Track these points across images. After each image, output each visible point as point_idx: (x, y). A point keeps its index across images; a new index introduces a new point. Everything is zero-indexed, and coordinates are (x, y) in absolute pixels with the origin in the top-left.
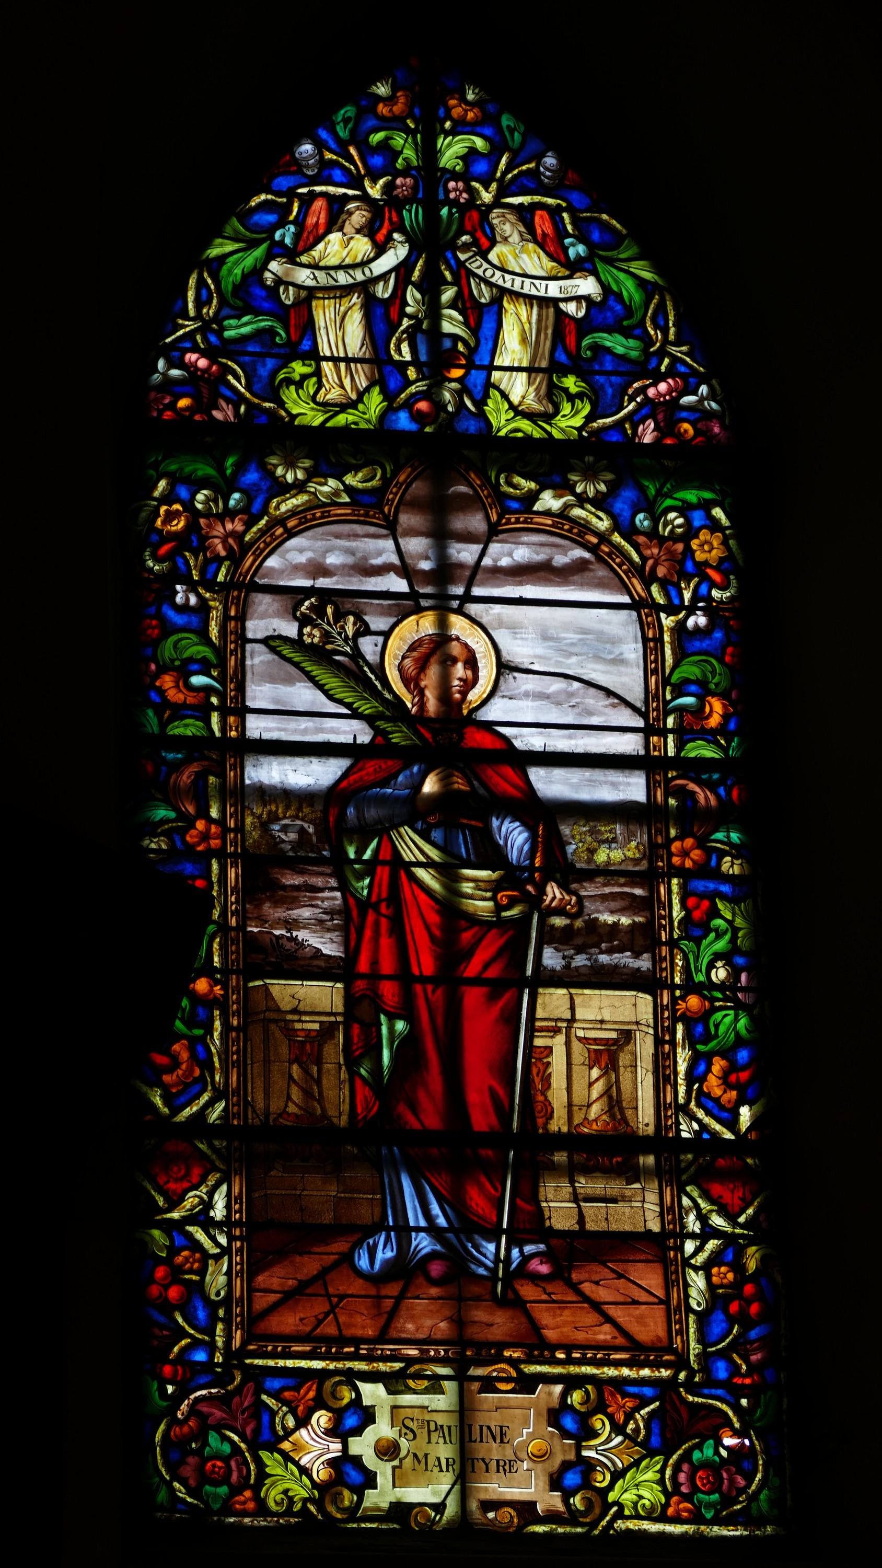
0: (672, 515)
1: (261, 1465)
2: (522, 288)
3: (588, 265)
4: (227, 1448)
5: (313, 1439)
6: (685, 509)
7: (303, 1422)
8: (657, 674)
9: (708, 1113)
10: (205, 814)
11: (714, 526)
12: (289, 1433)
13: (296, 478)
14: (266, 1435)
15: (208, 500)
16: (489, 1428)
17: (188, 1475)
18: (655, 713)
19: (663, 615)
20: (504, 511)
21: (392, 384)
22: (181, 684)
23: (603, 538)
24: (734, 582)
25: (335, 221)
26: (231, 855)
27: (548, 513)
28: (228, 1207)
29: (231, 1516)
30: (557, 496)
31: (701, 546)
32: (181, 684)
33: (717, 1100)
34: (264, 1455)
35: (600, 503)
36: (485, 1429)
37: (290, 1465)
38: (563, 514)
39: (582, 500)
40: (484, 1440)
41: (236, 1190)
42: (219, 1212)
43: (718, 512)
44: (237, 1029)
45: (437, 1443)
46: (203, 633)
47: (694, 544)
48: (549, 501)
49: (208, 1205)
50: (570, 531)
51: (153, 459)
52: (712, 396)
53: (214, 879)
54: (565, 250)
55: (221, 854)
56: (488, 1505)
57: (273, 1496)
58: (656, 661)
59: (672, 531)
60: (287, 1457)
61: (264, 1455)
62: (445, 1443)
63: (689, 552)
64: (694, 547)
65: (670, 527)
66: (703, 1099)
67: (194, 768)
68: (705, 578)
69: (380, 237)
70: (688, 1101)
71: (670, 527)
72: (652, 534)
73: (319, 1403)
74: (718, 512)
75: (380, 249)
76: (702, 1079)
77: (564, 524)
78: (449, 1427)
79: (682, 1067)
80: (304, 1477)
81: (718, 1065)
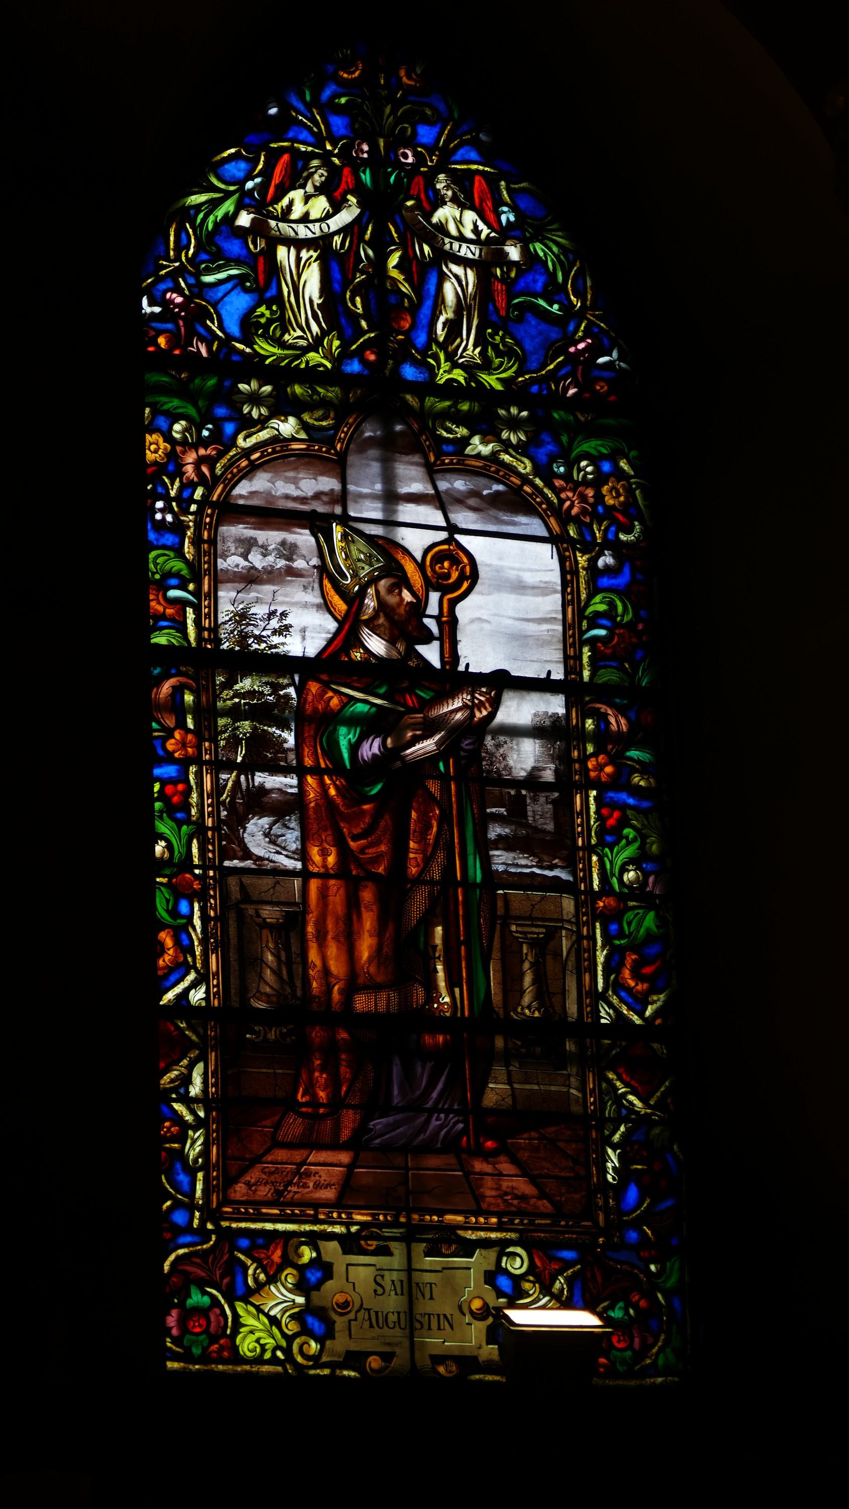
0: (584, 463)
1: (236, 1316)
2: (459, 251)
3: (517, 233)
4: (206, 1300)
5: (283, 1295)
6: (594, 460)
7: (273, 1279)
8: (573, 605)
9: (622, 1000)
10: (182, 724)
11: (619, 474)
12: (260, 1286)
13: (261, 414)
14: (240, 1291)
15: (185, 430)
16: (445, 1316)
17: (172, 1324)
18: (571, 640)
19: (578, 554)
20: (439, 454)
21: (349, 332)
22: (160, 596)
23: (524, 479)
24: (638, 527)
25: (295, 180)
26: (207, 763)
27: (478, 456)
28: (205, 1082)
29: (187, 960)
30: (484, 442)
31: (610, 491)
32: (160, 596)
33: (629, 990)
34: (240, 1307)
35: (522, 449)
36: (442, 1317)
37: (261, 1316)
38: (493, 457)
39: (507, 445)
40: (442, 1327)
41: (211, 1068)
42: (195, 1090)
43: (623, 464)
44: (215, 919)
45: (389, 1295)
46: (180, 554)
47: (605, 489)
48: (479, 446)
49: (187, 1080)
50: (497, 472)
51: (303, 1076)
52: (620, 359)
53: (192, 782)
54: (498, 215)
55: (198, 761)
56: (438, 1359)
57: (247, 1345)
58: (572, 593)
59: (585, 476)
60: (259, 1309)
61: (240, 1307)
62: (396, 1294)
63: (599, 497)
64: (604, 493)
65: (582, 473)
66: (618, 986)
67: (172, 681)
68: (614, 521)
69: (337, 194)
70: (606, 989)
71: (582, 473)
72: (567, 477)
73: (287, 1262)
74: (623, 464)
75: (337, 206)
76: (618, 972)
77: (491, 467)
78: (402, 1281)
79: (601, 958)
80: (274, 1328)
81: (631, 958)
